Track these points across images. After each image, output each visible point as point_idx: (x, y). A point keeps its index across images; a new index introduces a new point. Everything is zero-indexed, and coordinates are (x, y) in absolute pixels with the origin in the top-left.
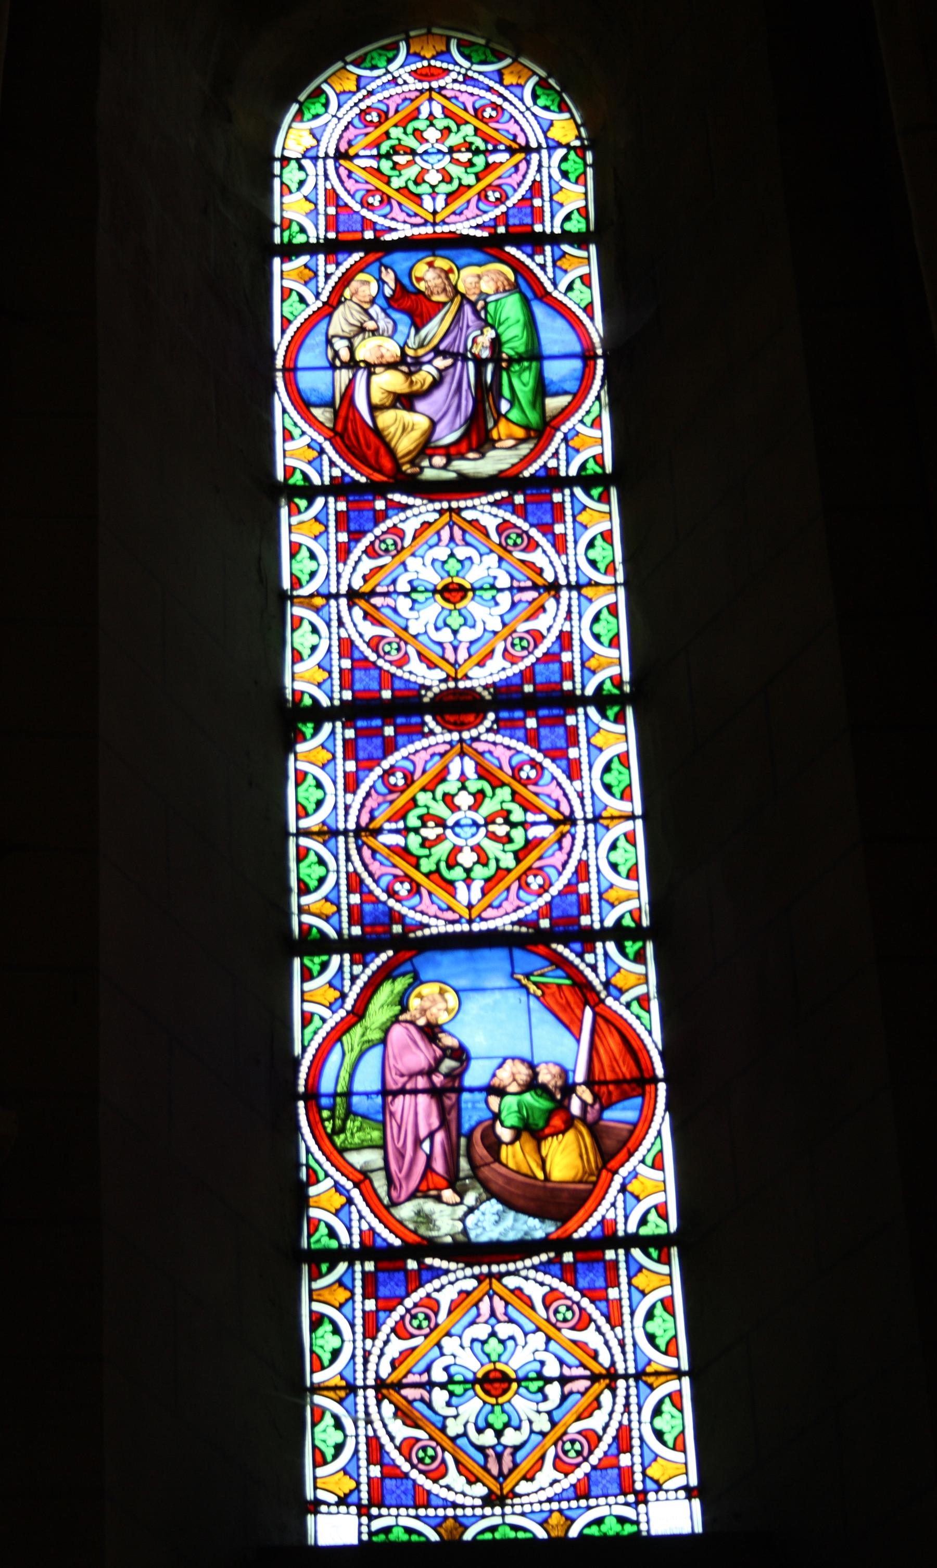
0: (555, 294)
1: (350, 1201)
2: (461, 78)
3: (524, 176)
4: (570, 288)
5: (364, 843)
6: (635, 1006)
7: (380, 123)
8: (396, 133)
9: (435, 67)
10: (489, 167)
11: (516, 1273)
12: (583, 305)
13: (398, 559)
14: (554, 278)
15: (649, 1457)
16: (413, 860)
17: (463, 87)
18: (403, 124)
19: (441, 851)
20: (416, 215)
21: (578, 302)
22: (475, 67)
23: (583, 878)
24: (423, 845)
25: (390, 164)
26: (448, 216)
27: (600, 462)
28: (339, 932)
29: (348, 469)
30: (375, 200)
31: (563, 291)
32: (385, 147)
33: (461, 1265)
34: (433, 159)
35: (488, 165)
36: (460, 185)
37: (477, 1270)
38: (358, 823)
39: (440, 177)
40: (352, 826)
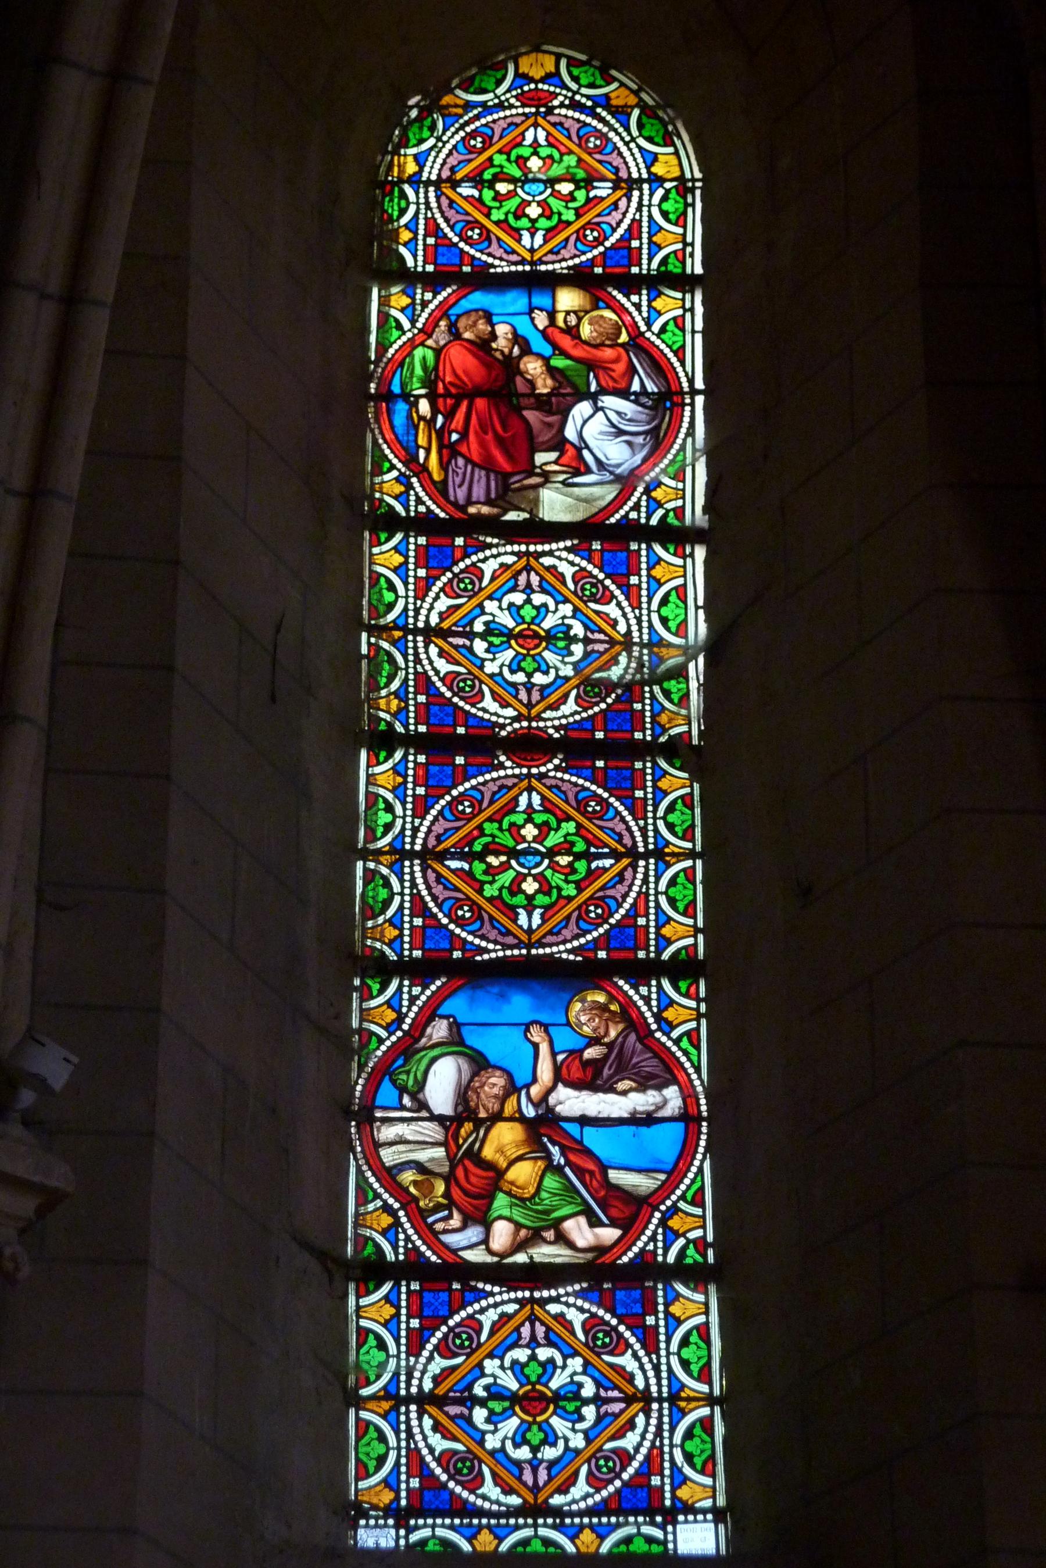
0: (648, 335)
1: (397, 1224)
2: (567, 102)
3: (624, 214)
4: (663, 330)
5: (443, 193)
6: (685, 1043)
7: (484, 149)
8: (499, 159)
9: (542, 90)
10: (592, 875)
11: (551, 553)
12: (675, 347)
13: (475, 601)
14: (649, 317)
15: (655, 229)
16: (485, 211)
17: (570, 113)
18: (505, 151)
19: (512, 204)
20: (514, 252)
21: (670, 343)
22: (584, 91)
23: (642, 913)
24: (494, 199)
25: (485, 645)
26: (546, 255)
27: (681, 325)
28: (400, 955)
29: (433, 507)
30: (475, 234)
31: (656, 332)
32: (487, 175)
33: (503, 542)
34: (532, 860)
35: (590, 872)
36: (560, 221)
37: (520, 1294)
38: (439, 175)
39: (540, 210)
40: (434, 177)
